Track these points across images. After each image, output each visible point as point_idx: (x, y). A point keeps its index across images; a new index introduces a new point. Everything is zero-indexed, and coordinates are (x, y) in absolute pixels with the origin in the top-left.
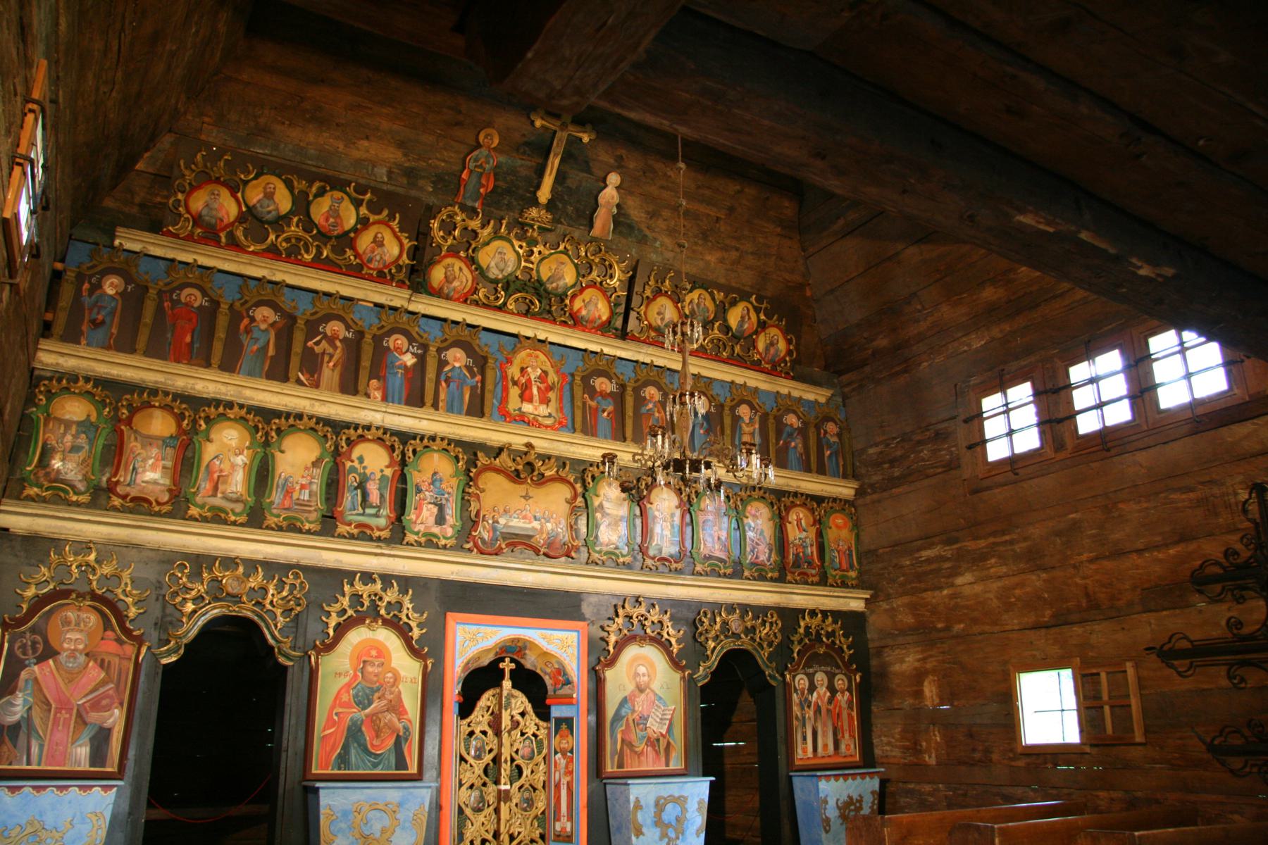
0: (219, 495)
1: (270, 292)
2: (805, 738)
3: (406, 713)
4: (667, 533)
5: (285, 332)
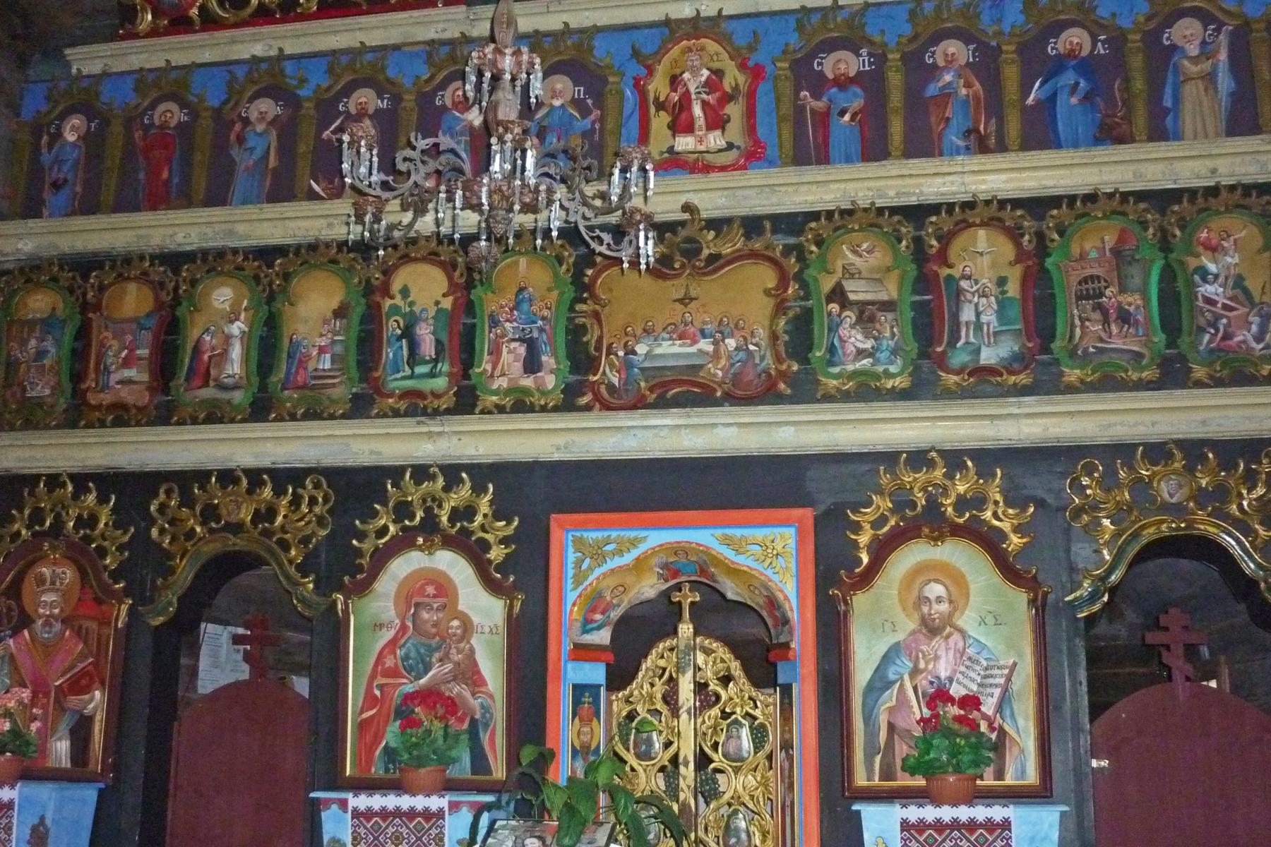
0: (212, 383)
1: (269, 78)
3: (483, 682)
4: (989, 318)
5: (287, 130)
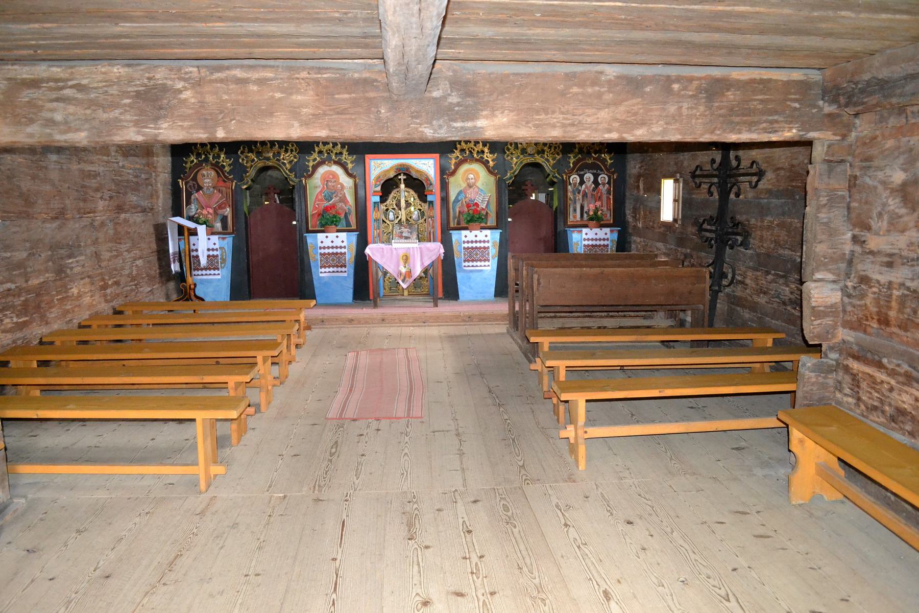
2: (575, 210)
